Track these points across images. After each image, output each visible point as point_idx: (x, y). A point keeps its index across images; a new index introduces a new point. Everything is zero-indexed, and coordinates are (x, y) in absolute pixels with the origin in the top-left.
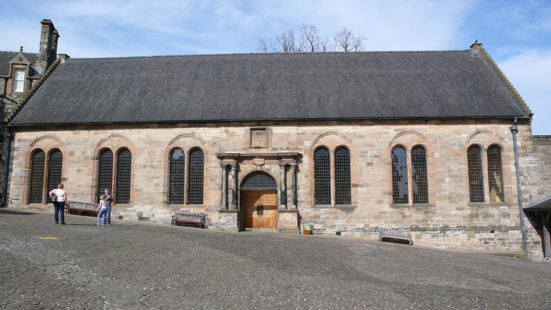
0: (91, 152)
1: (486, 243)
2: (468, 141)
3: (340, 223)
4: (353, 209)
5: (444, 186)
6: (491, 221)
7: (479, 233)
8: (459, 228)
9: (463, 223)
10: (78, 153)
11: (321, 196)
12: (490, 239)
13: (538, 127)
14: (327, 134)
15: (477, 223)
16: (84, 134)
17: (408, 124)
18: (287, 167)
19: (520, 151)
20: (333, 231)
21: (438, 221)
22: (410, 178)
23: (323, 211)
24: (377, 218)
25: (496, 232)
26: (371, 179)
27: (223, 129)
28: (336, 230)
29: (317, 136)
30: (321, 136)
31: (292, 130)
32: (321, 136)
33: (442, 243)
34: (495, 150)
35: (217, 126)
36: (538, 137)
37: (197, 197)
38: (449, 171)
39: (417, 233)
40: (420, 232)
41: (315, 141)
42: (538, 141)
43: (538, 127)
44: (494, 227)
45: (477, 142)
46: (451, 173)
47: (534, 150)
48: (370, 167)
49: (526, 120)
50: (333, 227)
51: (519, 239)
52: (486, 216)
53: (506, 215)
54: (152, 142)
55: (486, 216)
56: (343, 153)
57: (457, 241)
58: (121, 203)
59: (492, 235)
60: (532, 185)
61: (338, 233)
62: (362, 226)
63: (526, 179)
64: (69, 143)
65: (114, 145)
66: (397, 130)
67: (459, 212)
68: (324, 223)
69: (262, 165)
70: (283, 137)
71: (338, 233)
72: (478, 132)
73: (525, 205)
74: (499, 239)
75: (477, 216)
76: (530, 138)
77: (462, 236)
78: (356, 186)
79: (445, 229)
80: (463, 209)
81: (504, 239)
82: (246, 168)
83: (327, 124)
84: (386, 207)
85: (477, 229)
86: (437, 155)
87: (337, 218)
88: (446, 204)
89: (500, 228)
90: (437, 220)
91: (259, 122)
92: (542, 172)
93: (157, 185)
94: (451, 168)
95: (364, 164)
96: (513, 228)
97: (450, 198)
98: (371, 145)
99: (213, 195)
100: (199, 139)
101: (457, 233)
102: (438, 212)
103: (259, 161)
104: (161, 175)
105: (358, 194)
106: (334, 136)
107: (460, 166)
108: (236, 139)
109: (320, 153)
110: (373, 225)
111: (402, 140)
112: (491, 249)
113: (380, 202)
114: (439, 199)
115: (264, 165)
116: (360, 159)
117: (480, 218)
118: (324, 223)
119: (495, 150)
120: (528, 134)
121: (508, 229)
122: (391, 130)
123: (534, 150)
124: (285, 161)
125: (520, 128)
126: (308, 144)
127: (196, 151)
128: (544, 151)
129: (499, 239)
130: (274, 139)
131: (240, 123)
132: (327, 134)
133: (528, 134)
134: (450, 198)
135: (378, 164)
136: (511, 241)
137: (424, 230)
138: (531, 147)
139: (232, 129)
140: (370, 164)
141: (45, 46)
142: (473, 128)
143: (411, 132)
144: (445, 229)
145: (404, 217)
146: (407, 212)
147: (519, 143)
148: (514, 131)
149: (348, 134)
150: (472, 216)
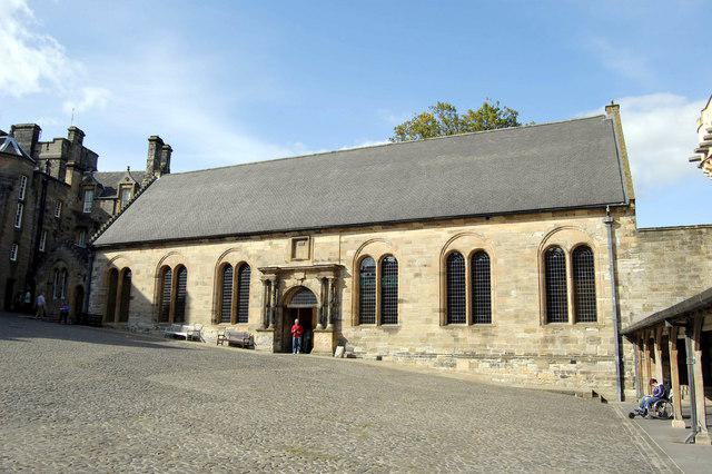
0: (153, 270)
1: (562, 377)
2: (544, 241)
3: (381, 347)
4: (397, 330)
5: (509, 301)
6: (572, 348)
7: (554, 363)
8: (528, 356)
9: (533, 351)
10: (143, 272)
11: (363, 316)
12: (569, 372)
13: (646, 217)
14: (372, 241)
15: (551, 349)
16: (149, 252)
17: (465, 224)
18: (325, 281)
19: (619, 251)
20: (373, 356)
21: (502, 346)
22: (467, 289)
23: (369, 330)
24: (424, 341)
25: (579, 363)
26: (420, 292)
27: (267, 241)
28: (377, 354)
29: (360, 245)
30: (365, 244)
31: (333, 239)
32: (365, 244)
33: (501, 376)
34: (583, 253)
35: (262, 239)
36: (645, 230)
37: (241, 316)
38: (516, 282)
39: (473, 361)
40: (476, 360)
41: (359, 251)
42: (646, 236)
43: (646, 217)
44: (577, 356)
45: (557, 242)
46: (519, 285)
47: (640, 249)
48: (417, 279)
49: (625, 208)
50: (374, 350)
51: (611, 373)
52: (566, 340)
53: (595, 340)
54: (205, 258)
55: (566, 340)
56: (480, 257)
57: (524, 374)
58: (482, 322)
59: (572, 367)
60: (634, 298)
61: (379, 358)
62: (407, 350)
63: (636, 287)
64: (137, 262)
65: (172, 263)
66: (452, 232)
67: (528, 336)
68: (364, 345)
69: (302, 280)
70: (326, 248)
71: (379, 358)
72: (558, 229)
73: (625, 326)
74: (583, 373)
75: (553, 340)
76: (634, 232)
77: (532, 367)
78: (402, 301)
79: (508, 357)
80: (534, 331)
81: (589, 373)
82: (290, 283)
83: (372, 231)
84: (435, 327)
85: (551, 358)
86: (501, 261)
87: (378, 340)
88: (511, 324)
89: (584, 358)
90: (499, 345)
91: (300, 231)
92: (651, 279)
93: (207, 302)
94: (520, 277)
95: (411, 275)
96: (604, 359)
97: (517, 316)
98: (420, 252)
99: (256, 313)
100: (246, 253)
101: (524, 362)
102: (500, 334)
103: (301, 275)
104: (533, 276)
105: (403, 310)
106: (380, 244)
107: (531, 274)
108: (275, 252)
109: (362, 264)
110: (419, 350)
111: (457, 245)
112: (570, 386)
113: (428, 321)
114: (502, 317)
115: (305, 278)
116: (407, 269)
117: (557, 343)
118: (364, 345)
119: (583, 253)
120: (631, 227)
121: (596, 359)
122: (442, 234)
123: (640, 249)
124: (323, 274)
125: (623, 220)
126: (351, 254)
127: (244, 266)
128: (654, 250)
129: (583, 373)
130: (316, 250)
131: (282, 233)
132: (372, 241)
133: (631, 227)
134: (517, 316)
135: (427, 275)
136: (599, 375)
137: (481, 357)
138: (634, 245)
139: (275, 242)
140: (417, 275)
141: (152, 163)
142: (550, 224)
143: (469, 233)
144: (508, 357)
145: (457, 340)
146: (461, 335)
147: (618, 242)
148: (612, 224)
149: (394, 239)
150: (546, 341)
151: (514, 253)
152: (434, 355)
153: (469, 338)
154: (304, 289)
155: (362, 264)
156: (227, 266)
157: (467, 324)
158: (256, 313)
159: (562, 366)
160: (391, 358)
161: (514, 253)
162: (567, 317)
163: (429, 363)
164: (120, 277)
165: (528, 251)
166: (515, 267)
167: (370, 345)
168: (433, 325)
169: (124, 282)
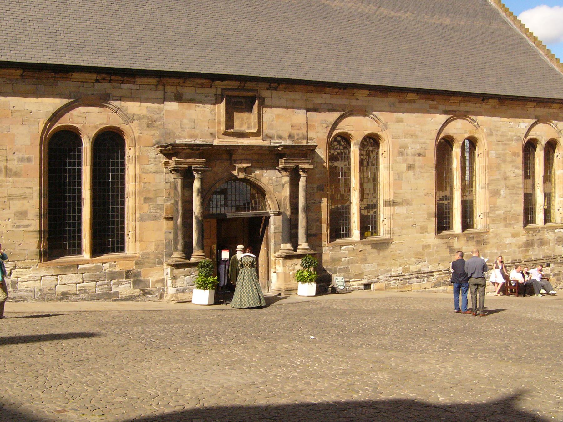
6: (546, 251)
25: (552, 265)
28: (365, 281)
44: (549, 258)
48: (411, 173)
50: (359, 275)
62: (400, 270)
71: (367, 286)
87: (364, 260)
93: (23, 214)
95: (404, 167)
98: (413, 136)
111: (533, 134)
113: (423, 230)
135: (421, 167)
140: (410, 167)
150: (529, 244)
152: (430, 274)
156: (345, 138)
157: (86, 255)
162: (80, 245)
163: (426, 283)
166: (505, 161)
167: (353, 269)
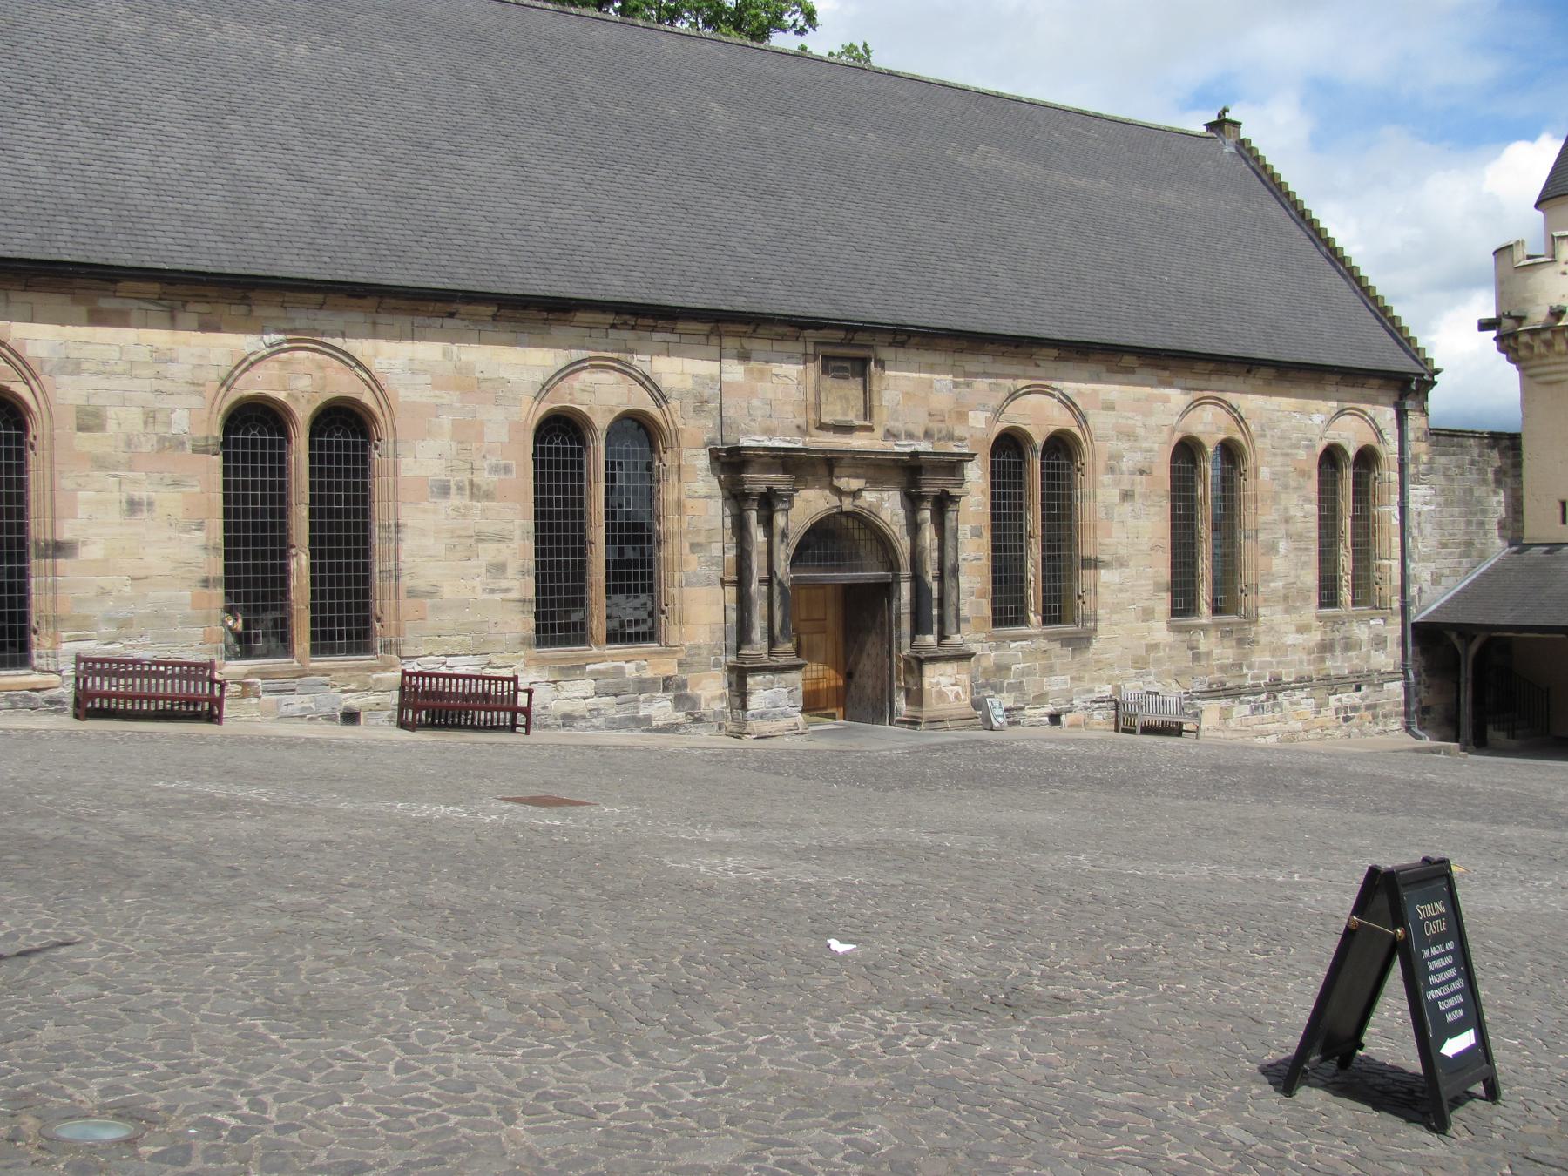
10: (123, 420)
12: (1355, 708)
20: (1039, 713)
23: (1028, 646)
26: (1126, 530)
28: (1049, 709)
38: (1287, 521)
43: (1443, 402)
48: (1127, 506)
50: (1041, 698)
54: (469, 385)
61: (1055, 719)
68: (1018, 687)
71: (1055, 719)
77: (1304, 702)
79: (1275, 687)
84: (1160, 630)
85: (1332, 684)
87: (1049, 670)
90: (1261, 665)
93: (498, 569)
97: (1286, 598)
108: (772, 398)
109: (1009, 445)
113: (1147, 614)
118: (1018, 687)
140: (1127, 496)
144: (1275, 687)
145: (1197, 657)
150: (1326, 648)
151: (456, 427)
153: (1217, 651)
154: (865, 523)
155: (1009, 445)
158: (699, 606)
159: (1344, 697)
160: (1078, 716)
161: (456, 427)
164: (1209, 469)
165: (1302, 454)
166: (1286, 487)
168: (1154, 624)
169: (279, 579)
